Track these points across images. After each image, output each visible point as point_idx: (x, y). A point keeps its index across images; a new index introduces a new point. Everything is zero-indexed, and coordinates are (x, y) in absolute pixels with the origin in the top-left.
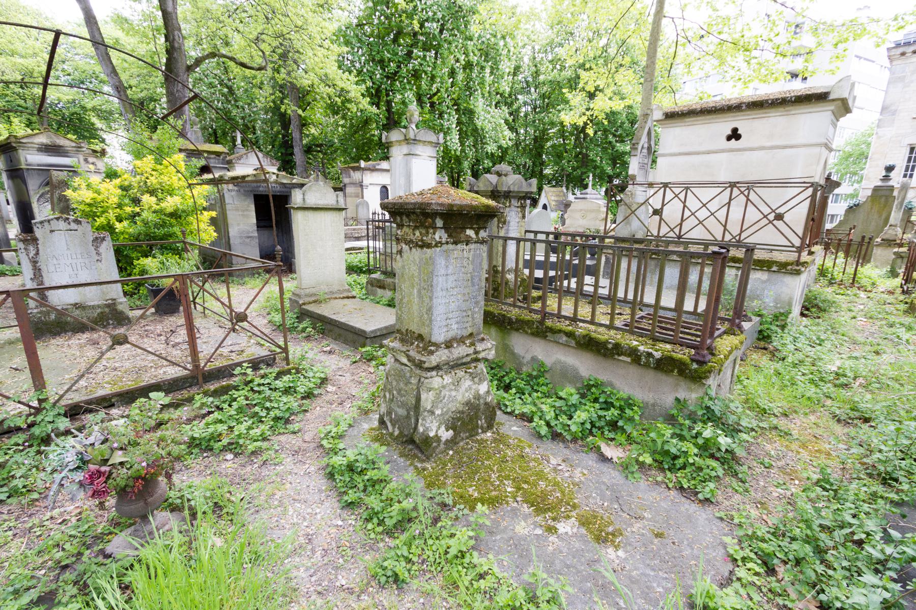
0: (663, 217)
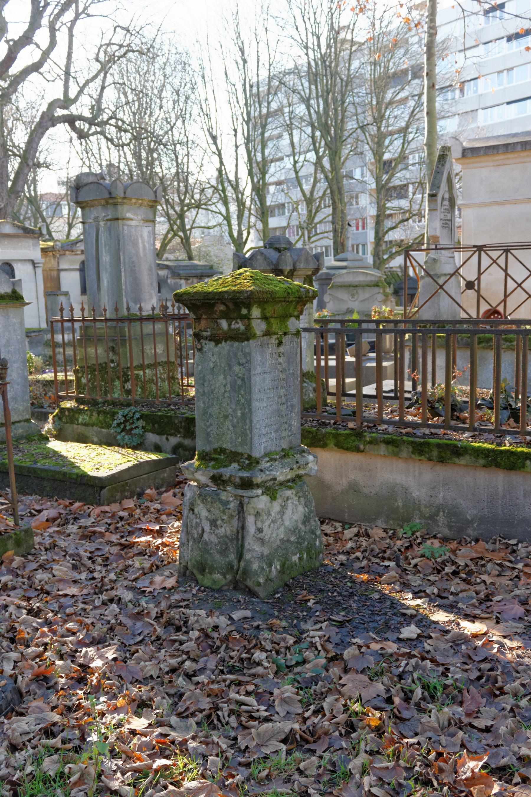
0: (482, 293)
